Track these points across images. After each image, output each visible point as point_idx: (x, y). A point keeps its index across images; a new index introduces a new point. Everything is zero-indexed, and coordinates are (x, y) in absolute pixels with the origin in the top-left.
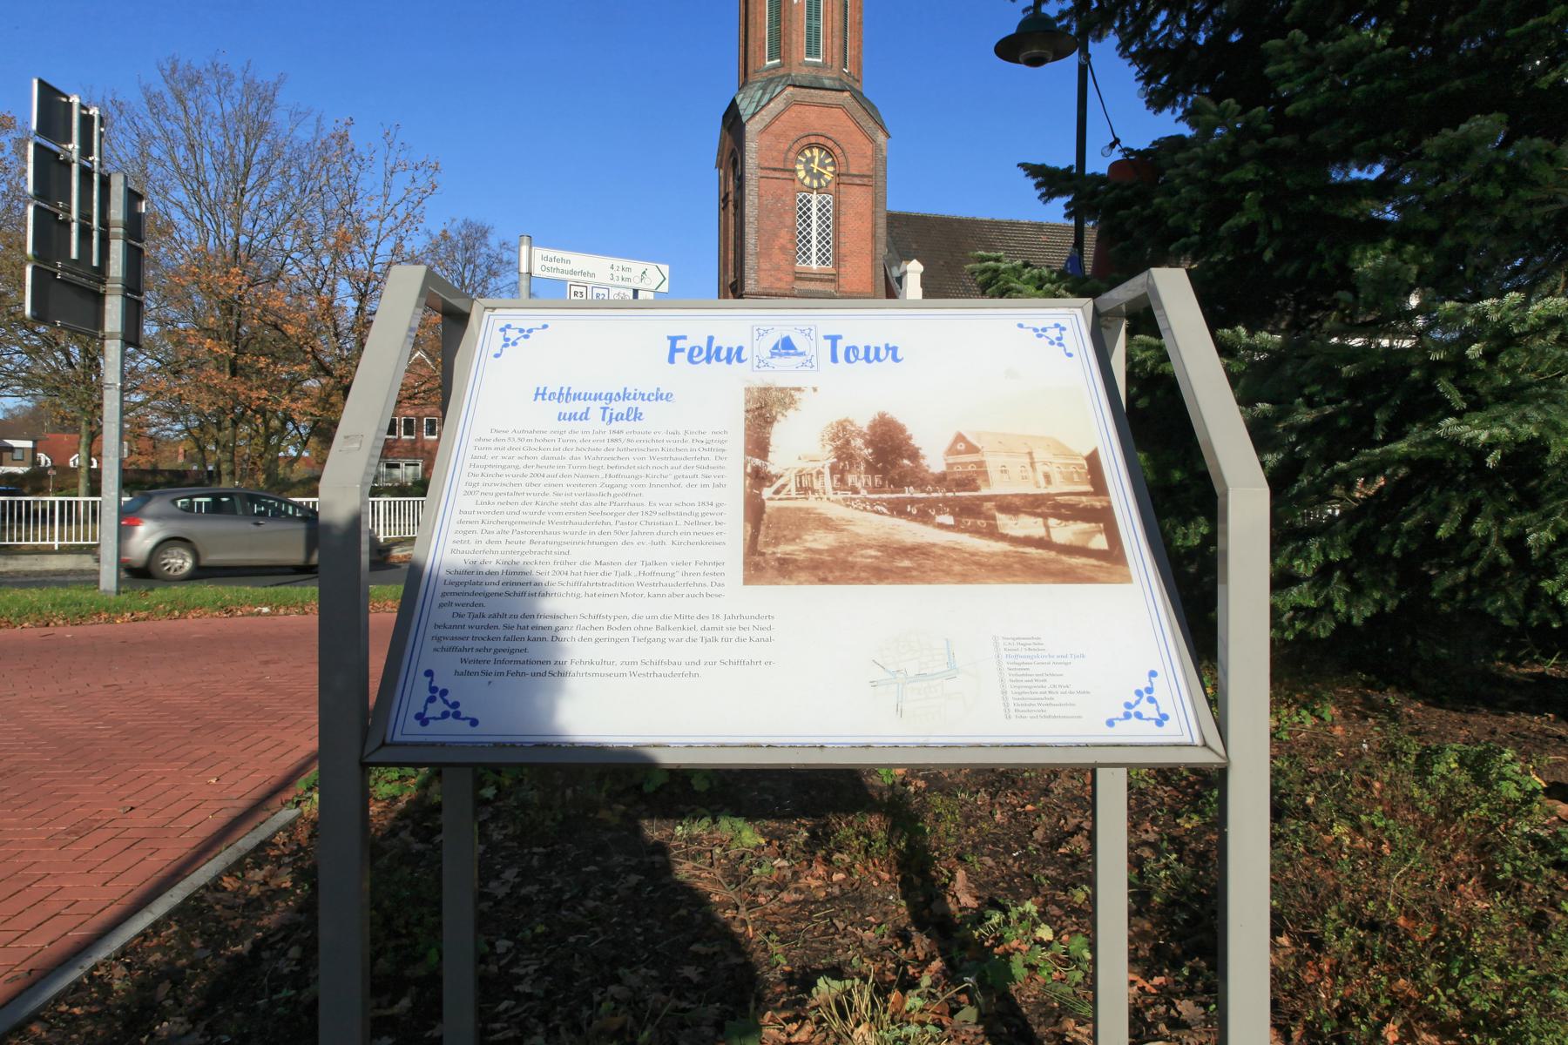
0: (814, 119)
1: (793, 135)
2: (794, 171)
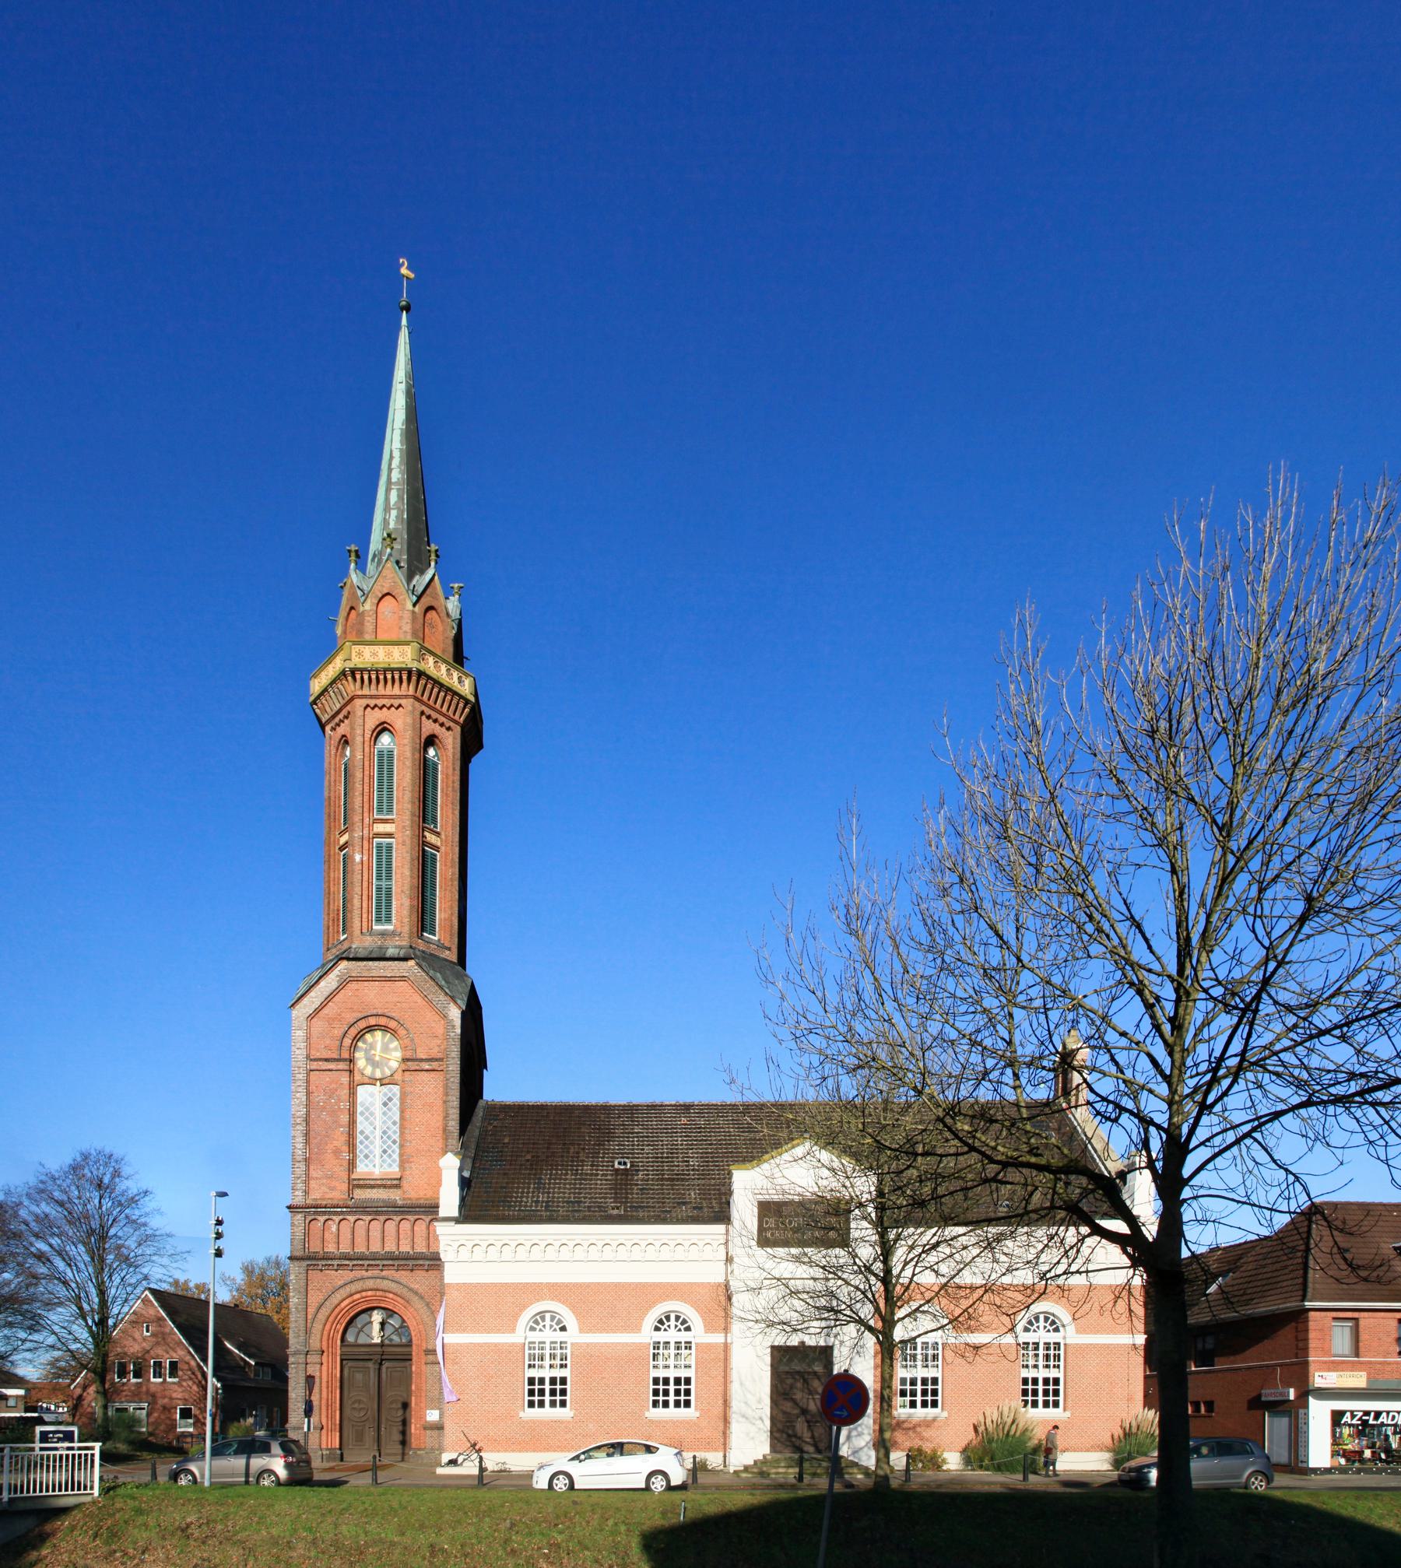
0: (373, 996)
1: (351, 1017)
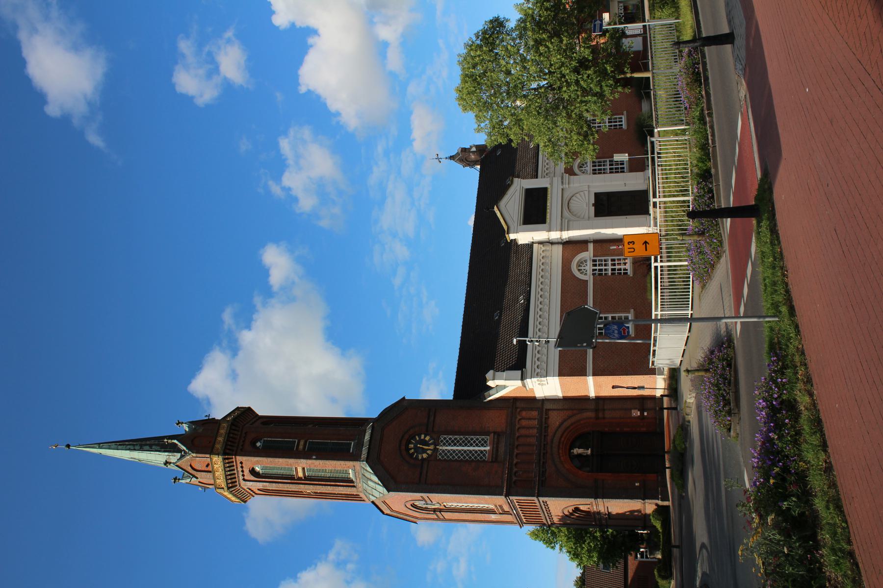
2: (423, 459)
